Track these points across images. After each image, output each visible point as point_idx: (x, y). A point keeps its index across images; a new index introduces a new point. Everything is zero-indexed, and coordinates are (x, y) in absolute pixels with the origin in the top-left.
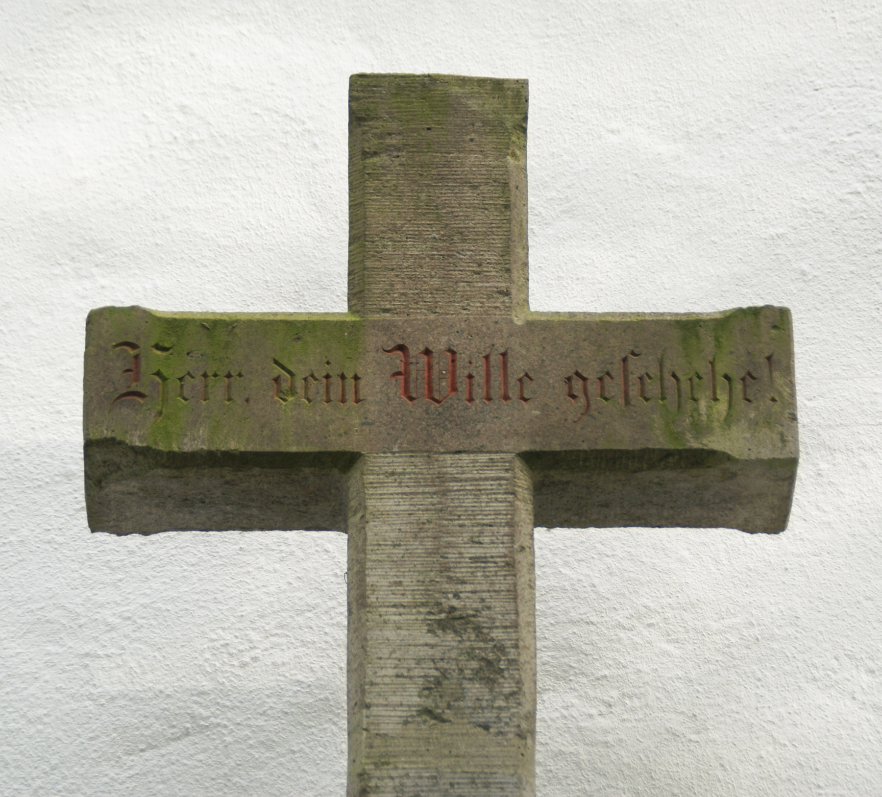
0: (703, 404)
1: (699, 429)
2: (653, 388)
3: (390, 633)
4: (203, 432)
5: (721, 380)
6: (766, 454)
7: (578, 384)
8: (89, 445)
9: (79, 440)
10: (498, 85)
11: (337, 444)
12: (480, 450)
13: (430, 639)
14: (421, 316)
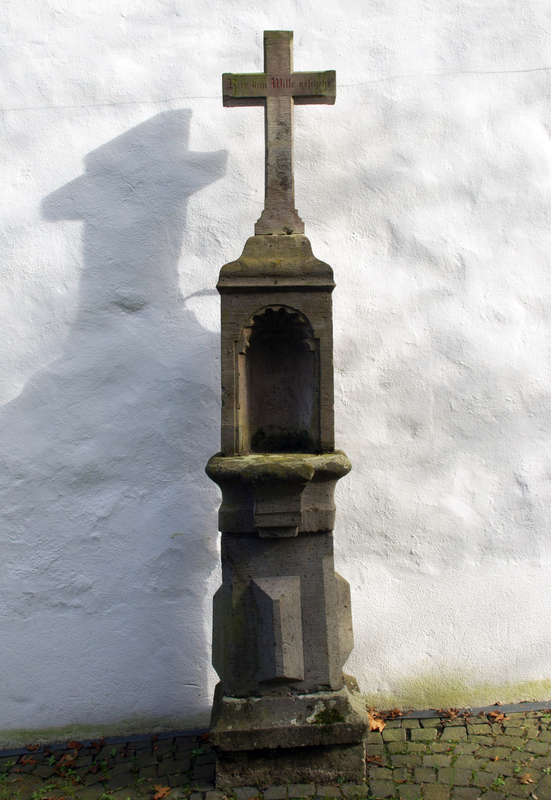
0: (321, 87)
1: (320, 91)
2: (313, 85)
3: (271, 126)
4: (241, 94)
5: (324, 83)
6: (331, 95)
7: (301, 84)
8: (223, 96)
9: (222, 95)
10: (288, 32)
11: (263, 95)
12: (285, 96)
13: (278, 127)
14: (276, 73)
